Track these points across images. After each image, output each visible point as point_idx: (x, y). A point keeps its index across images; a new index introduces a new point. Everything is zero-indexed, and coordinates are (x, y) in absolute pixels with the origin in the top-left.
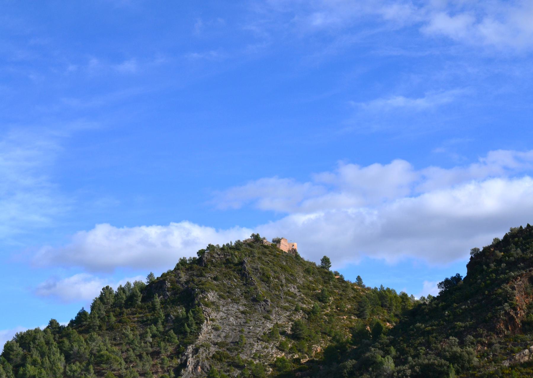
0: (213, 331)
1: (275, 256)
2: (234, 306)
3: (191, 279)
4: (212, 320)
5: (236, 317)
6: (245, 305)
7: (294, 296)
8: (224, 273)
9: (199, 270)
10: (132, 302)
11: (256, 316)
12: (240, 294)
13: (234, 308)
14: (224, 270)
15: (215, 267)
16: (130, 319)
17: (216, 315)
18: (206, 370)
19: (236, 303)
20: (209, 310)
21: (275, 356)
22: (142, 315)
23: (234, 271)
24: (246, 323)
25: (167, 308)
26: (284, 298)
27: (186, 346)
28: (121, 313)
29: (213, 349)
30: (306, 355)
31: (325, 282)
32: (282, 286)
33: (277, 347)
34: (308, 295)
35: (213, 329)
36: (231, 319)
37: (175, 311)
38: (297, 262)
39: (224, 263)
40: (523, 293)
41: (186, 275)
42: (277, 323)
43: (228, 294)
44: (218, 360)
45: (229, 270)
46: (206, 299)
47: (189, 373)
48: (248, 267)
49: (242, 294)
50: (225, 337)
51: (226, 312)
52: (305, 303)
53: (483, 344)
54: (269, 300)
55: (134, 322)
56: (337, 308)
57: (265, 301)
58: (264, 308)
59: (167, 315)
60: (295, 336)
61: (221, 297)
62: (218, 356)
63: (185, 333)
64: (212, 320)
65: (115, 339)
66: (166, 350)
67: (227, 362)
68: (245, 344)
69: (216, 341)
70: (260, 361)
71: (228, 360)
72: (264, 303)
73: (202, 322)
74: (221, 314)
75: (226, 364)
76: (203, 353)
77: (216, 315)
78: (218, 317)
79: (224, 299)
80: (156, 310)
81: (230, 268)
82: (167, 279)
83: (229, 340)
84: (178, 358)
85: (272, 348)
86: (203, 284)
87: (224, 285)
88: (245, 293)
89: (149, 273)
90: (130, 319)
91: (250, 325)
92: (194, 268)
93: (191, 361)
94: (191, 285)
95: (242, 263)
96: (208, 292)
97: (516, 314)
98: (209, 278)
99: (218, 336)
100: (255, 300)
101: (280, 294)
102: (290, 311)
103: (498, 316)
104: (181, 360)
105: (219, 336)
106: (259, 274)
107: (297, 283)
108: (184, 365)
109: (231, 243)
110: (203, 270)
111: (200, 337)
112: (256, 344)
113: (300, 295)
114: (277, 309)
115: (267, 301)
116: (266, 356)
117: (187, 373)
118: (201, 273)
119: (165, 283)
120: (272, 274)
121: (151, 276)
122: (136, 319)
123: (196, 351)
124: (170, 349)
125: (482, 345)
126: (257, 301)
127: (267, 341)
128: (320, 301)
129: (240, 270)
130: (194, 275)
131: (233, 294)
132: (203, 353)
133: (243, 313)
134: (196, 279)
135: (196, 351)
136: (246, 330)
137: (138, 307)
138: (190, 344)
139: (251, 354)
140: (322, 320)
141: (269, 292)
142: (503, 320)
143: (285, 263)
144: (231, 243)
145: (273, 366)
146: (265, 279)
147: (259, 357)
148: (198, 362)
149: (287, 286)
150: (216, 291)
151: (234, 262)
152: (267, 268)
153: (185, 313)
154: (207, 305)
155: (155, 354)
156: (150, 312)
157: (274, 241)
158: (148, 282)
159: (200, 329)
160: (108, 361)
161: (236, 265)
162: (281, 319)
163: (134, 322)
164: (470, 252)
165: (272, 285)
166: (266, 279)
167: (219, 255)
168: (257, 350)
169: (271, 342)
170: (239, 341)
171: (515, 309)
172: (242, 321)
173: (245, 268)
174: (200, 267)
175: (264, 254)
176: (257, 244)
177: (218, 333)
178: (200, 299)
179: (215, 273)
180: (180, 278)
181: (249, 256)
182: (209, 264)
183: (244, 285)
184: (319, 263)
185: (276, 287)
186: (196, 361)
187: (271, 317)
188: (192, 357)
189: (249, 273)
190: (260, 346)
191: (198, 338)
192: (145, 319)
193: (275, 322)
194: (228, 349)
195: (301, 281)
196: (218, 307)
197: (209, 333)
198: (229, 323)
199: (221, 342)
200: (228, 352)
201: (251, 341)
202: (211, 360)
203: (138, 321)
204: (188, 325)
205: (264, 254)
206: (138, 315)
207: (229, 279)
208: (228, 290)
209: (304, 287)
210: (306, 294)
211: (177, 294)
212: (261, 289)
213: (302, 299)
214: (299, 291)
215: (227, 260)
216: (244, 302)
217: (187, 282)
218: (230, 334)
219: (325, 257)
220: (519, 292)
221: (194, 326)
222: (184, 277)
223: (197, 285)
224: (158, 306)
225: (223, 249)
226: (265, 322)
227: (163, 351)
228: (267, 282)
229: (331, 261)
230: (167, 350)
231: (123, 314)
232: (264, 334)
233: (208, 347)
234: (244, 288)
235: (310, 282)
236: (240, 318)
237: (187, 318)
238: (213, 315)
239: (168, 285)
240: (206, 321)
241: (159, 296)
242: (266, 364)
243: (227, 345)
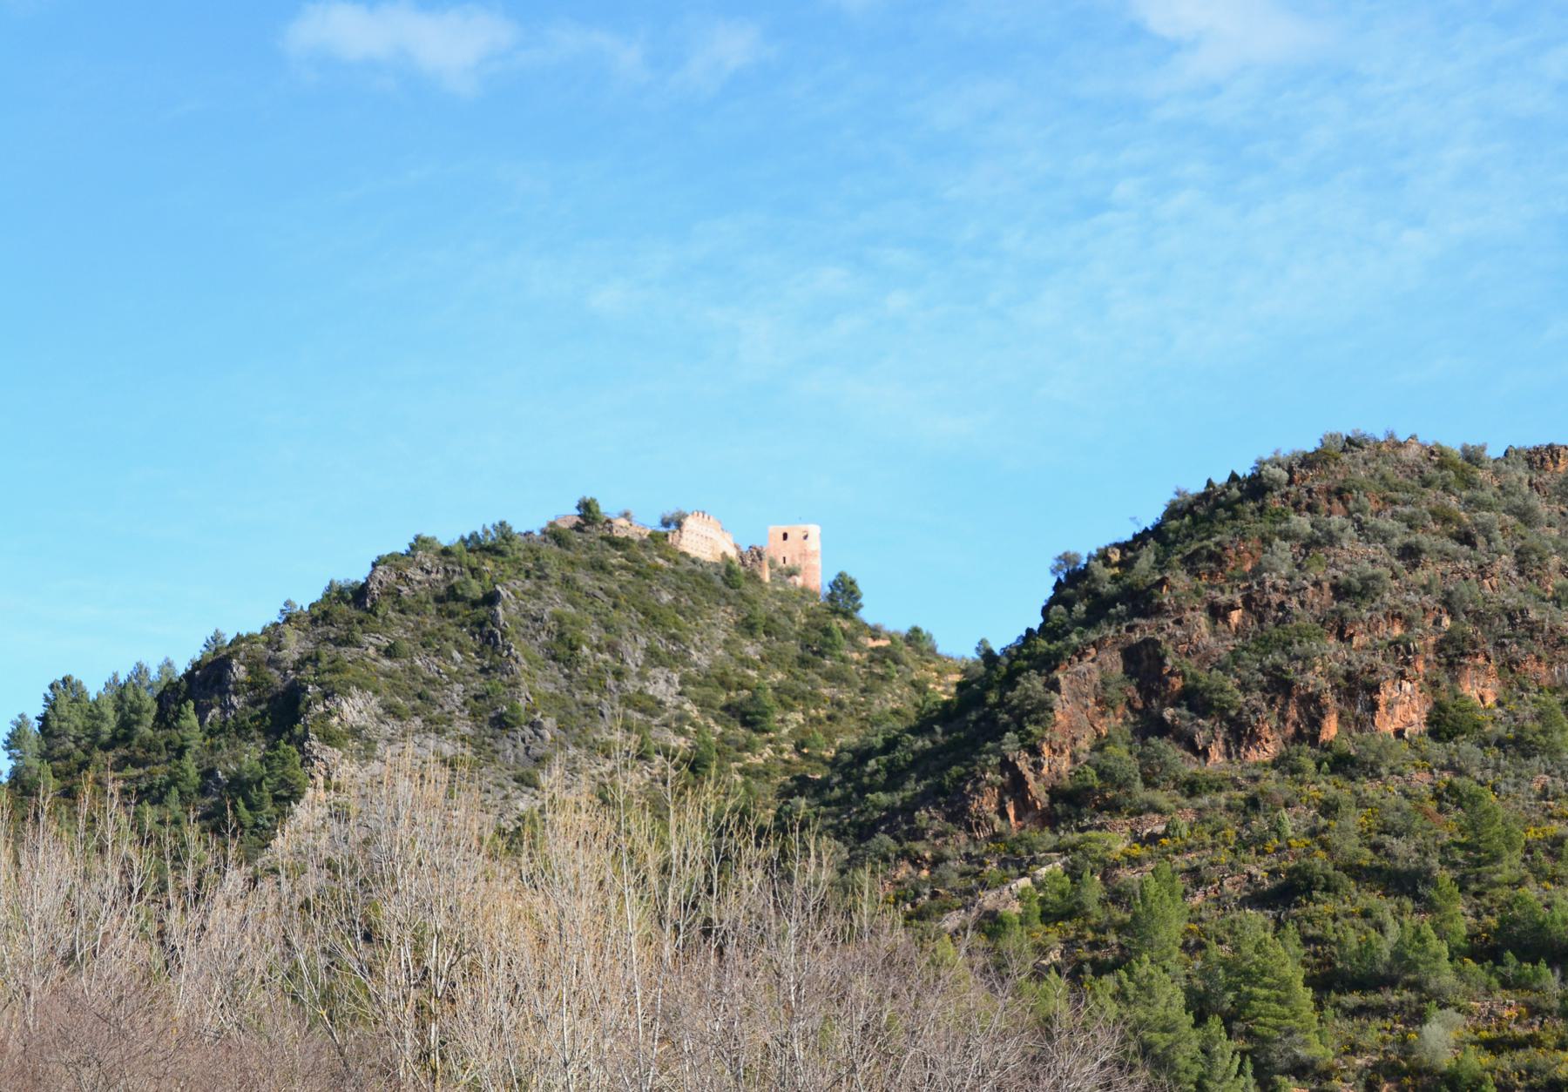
7: (652, 707)
12: (458, 701)
14: (430, 622)
15: (402, 611)
19: (437, 732)
20: (332, 754)
39: (439, 599)
40: (1091, 702)
41: (307, 638)
46: (335, 720)
49: (465, 704)
53: (916, 861)
56: (798, 748)
58: (527, 749)
61: (392, 711)
72: (528, 731)
73: (296, 796)
79: (399, 717)
81: (451, 614)
87: (413, 670)
89: (211, 633)
95: (491, 599)
96: (346, 694)
97: (1037, 766)
98: (372, 651)
101: (600, 704)
103: (979, 774)
106: (544, 636)
110: (360, 622)
111: (279, 842)
114: (572, 751)
115: (540, 725)
119: (230, 667)
120: (593, 634)
125: (913, 863)
128: (745, 724)
129: (481, 624)
142: (992, 785)
143: (666, 597)
146: (563, 650)
149: (642, 676)
151: (470, 595)
154: (329, 739)
164: (1051, 562)
165: (582, 671)
166: (563, 651)
167: (428, 572)
171: (1035, 751)
175: (599, 567)
181: (528, 577)
183: (483, 671)
185: (595, 681)
196: (370, 744)
205: (599, 567)
207: (438, 653)
209: (705, 680)
210: (704, 705)
213: (682, 718)
216: (465, 727)
217: (299, 665)
220: (1077, 695)
222: (294, 645)
228: (568, 663)
229: (862, 586)
235: (745, 662)
239: (239, 672)
241: (201, 711)
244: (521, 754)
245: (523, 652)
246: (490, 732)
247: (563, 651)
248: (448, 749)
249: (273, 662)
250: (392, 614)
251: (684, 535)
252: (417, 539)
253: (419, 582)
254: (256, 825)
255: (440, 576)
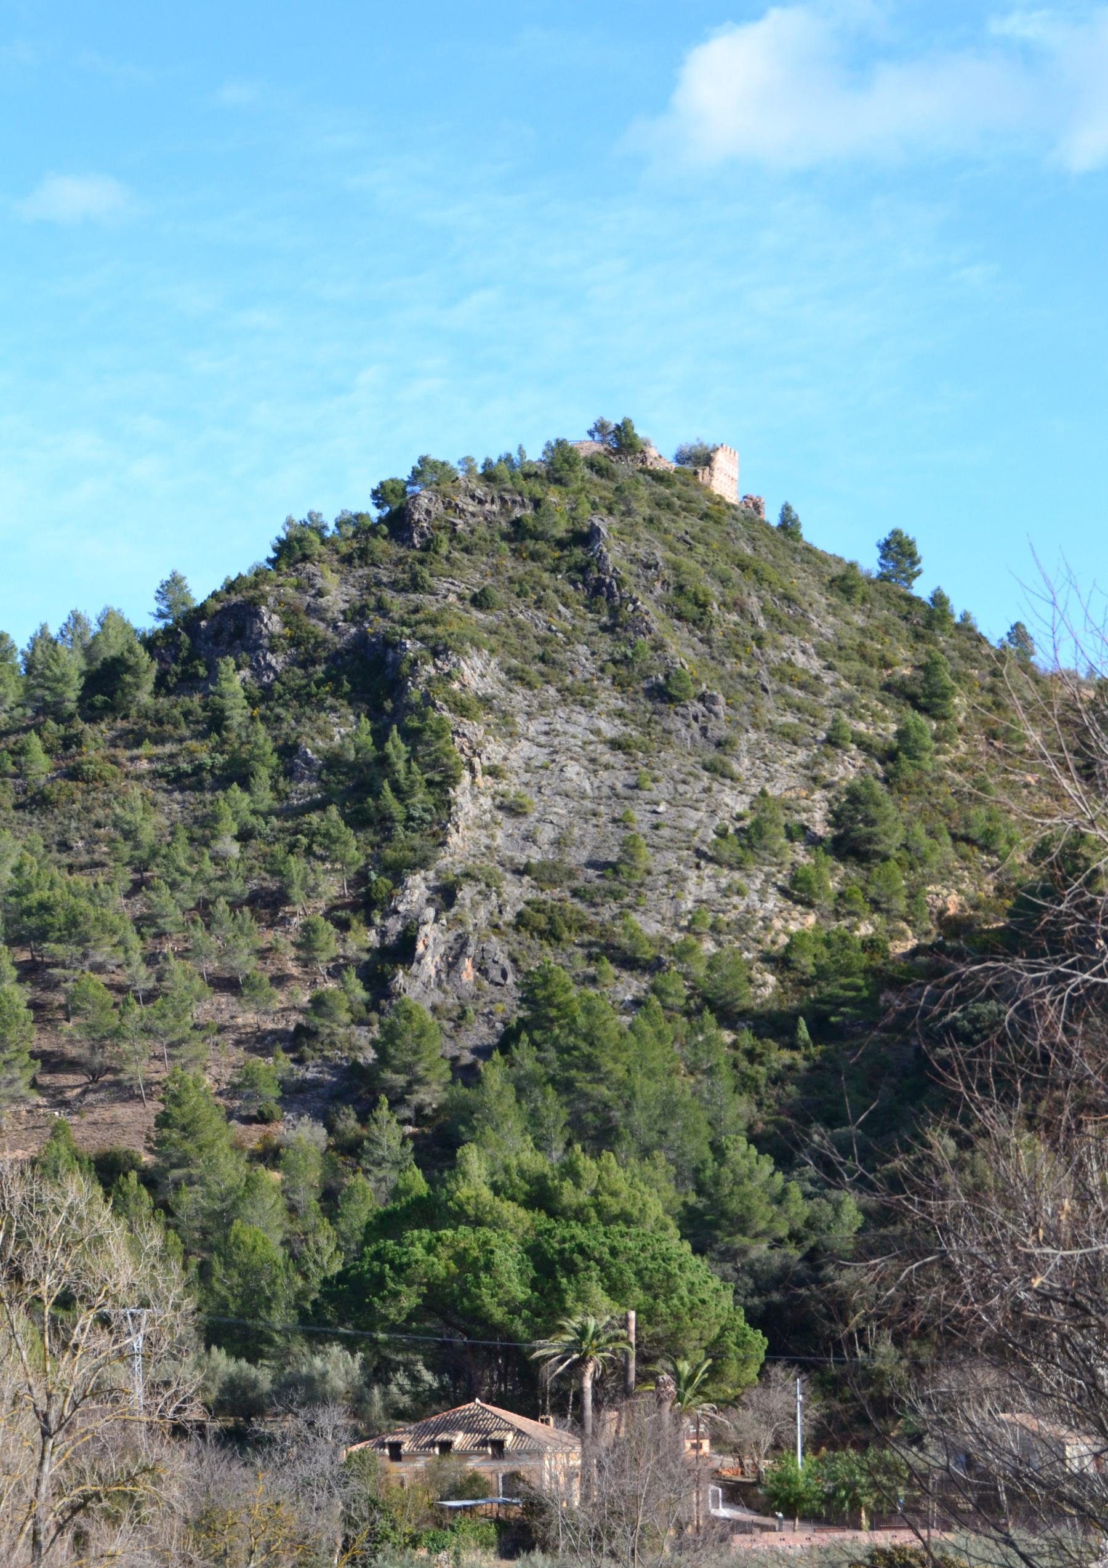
0: (500, 816)
1: (705, 516)
2: (574, 716)
3: (372, 602)
4: (493, 772)
5: (593, 761)
6: (620, 714)
8: (511, 580)
9: (401, 561)
10: (111, 695)
11: (673, 760)
12: (591, 667)
13: (576, 725)
15: (467, 550)
16: (116, 763)
17: (503, 750)
18: (495, 974)
19: (583, 704)
20: (474, 729)
21: (778, 924)
22: (169, 748)
23: (554, 570)
24: (636, 787)
25: (279, 719)
26: (777, 692)
27: (397, 873)
28: (71, 742)
29: (516, 893)
30: (903, 925)
31: (918, 637)
32: (759, 640)
33: (783, 891)
34: (868, 684)
35: (500, 808)
36: (572, 770)
37: (321, 732)
38: (795, 550)
39: (505, 537)
42: (763, 793)
43: (540, 666)
44: (542, 934)
45: (531, 565)
46: (456, 686)
47: (426, 985)
48: (613, 555)
50: (558, 843)
51: (543, 739)
52: (861, 718)
54: (721, 699)
55: (139, 778)
57: (702, 698)
58: (704, 730)
59: (288, 751)
60: (849, 844)
61: (515, 676)
62: (542, 921)
63: (383, 824)
64: (493, 772)
65: (64, 846)
66: (311, 892)
67: (581, 945)
68: (649, 873)
69: (521, 859)
70: (719, 944)
71: (586, 937)
72: (699, 707)
73: (454, 781)
74: (525, 748)
75: (580, 952)
76: (475, 905)
77: (503, 750)
78: (516, 761)
79: (530, 685)
80: (228, 729)
81: (535, 556)
82: (263, 596)
83: (577, 857)
84: (369, 923)
85: (762, 895)
86: (434, 622)
87: (519, 627)
88: (615, 662)
90: (116, 763)
91: (655, 795)
92: (378, 553)
93: (432, 940)
94: (377, 625)
95: (586, 538)
98: (452, 598)
99: (526, 838)
100: (663, 694)
101: (758, 675)
102: (808, 746)
104: (383, 934)
105: (529, 838)
106: (658, 589)
107: (810, 632)
108: (403, 950)
109: (521, 451)
110: (422, 562)
111: (454, 839)
112: (692, 874)
113: (836, 684)
114: (753, 735)
115: (713, 700)
116: (742, 926)
117: (418, 986)
118: (414, 577)
119: (258, 615)
120: (714, 589)
121: (172, 587)
122: (144, 765)
123: (445, 895)
124: (333, 887)
126: (672, 699)
127: (738, 865)
129: (583, 569)
130: (379, 584)
131: (562, 666)
132: (475, 905)
133: (615, 745)
134: (397, 603)
135: (445, 895)
136: (640, 816)
137: (144, 714)
138: (414, 867)
139: (677, 914)
140: (944, 788)
141: (712, 664)
143: (749, 551)
144: (521, 451)
145: (780, 962)
146: (689, 609)
147: (714, 928)
148: (462, 942)
150: (492, 651)
152: (692, 564)
153: (366, 739)
154: (462, 709)
155: (269, 904)
156: (202, 736)
157: (681, 458)
158: (161, 615)
159: (446, 805)
160: (73, 929)
161: (561, 544)
162: (780, 778)
163: (139, 778)
166: (691, 610)
167: (481, 502)
168: (699, 901)
169: (752, 868)
170: (621, 861)
172: (620, 779)
173: (602, 558)
174: (402, 552)
176: (624, 467)
177: (525, 824)
178: (429, 681)
179: (472, 576)
180: (320, 594)
181: (610, 512)
182: (443, 536)
183: (604, 629)
184: (870, 562)
185: (733, 645)
186: (451, 936)
187: (735, 767)
188: (436, 920)
189: (621, 583)
190: (709, 886)
191: (444, 844)
192: (185, 767)
193: (756, 790)
194: (575, 893)
195: (825, 625)
196: (506, 717)
197: (485, 827)
198: (567, 786)
199: (543, 865)
200: (580, 906)
201: (670, 860)
202: (513, 936)
203: (156, 775)
204: (396, 789)
206: (148, 748)
207: (539, 603)
208: (538, 650)
211: (314, 662)
212: (682, 650)
214: (830, 668)
215: (517, 523)
217: (357, 614)
218: (576, 832)
219: (895, 533)
221: (420, 798)
222: (337, 593)
223: (404, 623)
224: (237, 712)
225: (489, 476)
226: (715, 786)
227: (296, 893)
229: (920, 550)
230: (314, 889)
231: (79, 744)
232: (722, 834)
233: (490, 885)
234: (605, 643)
236: (607, 767)
237: (383, 761)
238: (494, 751)
239: (273, 623)
240: (466, 774)
242: (746, 955)
243: (571, 874)
244: (697, 736)
245: (649, 606)
246: (650, 706)
247: (691, 610)
248: (610, 729)
249: (311, 611)
250: (456, 555)
251: (716, 473)
252: (423, 461)
253: (473, 515)
254: (410, 818)
255: (495, 508)
